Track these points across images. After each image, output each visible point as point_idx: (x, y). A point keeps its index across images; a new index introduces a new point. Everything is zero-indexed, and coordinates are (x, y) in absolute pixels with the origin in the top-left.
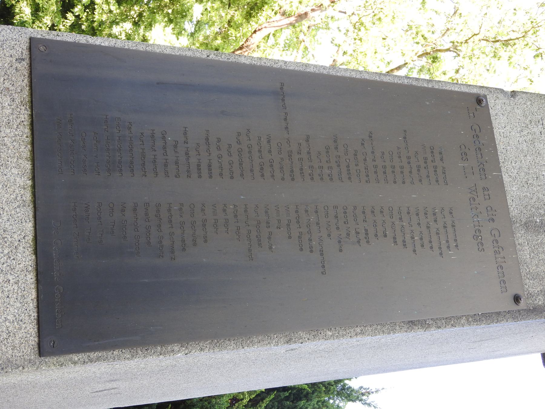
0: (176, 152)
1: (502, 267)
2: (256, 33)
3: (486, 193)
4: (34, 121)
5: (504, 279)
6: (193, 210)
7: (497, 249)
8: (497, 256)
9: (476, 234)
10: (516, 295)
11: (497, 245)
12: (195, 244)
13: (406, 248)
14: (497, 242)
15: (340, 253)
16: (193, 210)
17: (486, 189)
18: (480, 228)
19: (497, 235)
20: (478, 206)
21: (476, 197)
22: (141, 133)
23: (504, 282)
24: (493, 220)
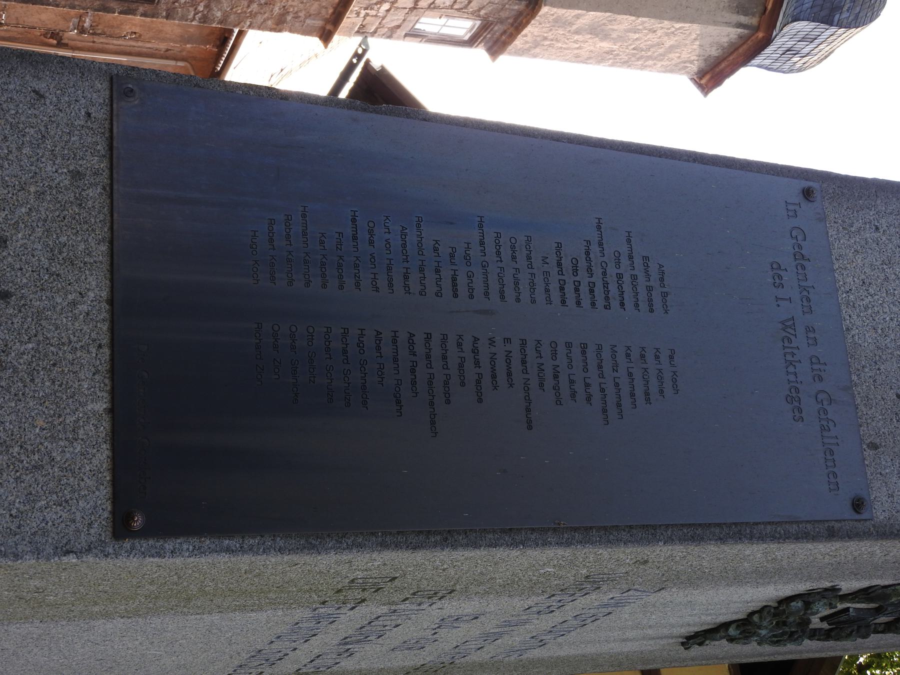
0: (673, 366)
1: (832, 453)
2: (382, 67)
3: (811, 335)
4: (114, 221)
5: (835, 470)
6: (312, 336)
7: (825, 423)
8: (826, 434)
9: (790, 395)
10: (863, 498)
11: (831, 458)
12: (648, 400)
13: (650, 403)
14: (826, 412)
15: (447, 405)
16: (312, 336)
17: (811, 329)
18: (798, 386)
19: (799, 238)
20: (795, 351)
21: (792, 337)
22: (323, 255)
23: (835, 475)
24: (821, 379)
